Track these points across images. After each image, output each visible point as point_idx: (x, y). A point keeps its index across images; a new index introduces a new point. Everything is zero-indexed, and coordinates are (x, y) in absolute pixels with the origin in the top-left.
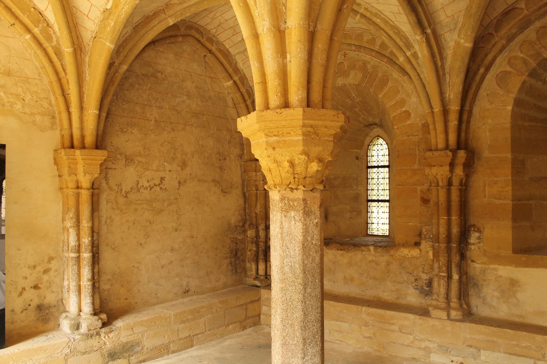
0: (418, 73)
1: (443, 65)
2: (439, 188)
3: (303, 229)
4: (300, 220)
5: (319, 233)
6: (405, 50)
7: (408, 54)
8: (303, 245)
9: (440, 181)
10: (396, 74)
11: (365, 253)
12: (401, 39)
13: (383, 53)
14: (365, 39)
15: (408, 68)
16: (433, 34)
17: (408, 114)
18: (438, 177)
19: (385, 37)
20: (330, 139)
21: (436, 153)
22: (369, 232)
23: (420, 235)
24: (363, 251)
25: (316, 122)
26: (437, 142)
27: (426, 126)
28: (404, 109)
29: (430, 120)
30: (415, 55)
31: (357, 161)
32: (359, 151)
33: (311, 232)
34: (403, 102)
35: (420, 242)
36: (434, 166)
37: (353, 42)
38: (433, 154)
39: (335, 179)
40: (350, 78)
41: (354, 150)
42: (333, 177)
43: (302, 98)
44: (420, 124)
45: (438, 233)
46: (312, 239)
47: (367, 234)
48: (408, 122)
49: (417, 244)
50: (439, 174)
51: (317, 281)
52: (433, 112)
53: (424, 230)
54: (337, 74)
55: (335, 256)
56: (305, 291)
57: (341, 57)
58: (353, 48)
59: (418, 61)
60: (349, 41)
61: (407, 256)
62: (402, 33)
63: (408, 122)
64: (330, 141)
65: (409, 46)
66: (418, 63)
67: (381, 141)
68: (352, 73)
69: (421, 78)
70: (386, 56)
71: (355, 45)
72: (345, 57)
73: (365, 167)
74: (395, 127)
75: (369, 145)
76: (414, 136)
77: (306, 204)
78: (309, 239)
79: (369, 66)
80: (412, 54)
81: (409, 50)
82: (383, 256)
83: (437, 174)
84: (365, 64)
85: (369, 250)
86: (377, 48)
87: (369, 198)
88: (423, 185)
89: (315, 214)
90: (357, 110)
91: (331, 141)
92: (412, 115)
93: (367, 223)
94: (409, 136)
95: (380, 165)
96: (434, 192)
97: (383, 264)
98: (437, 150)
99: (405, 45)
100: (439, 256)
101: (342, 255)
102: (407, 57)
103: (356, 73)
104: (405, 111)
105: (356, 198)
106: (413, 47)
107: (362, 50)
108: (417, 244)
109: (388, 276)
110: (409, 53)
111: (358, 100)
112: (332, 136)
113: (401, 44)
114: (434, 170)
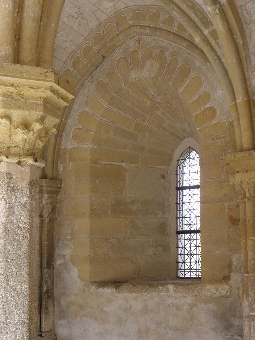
0: (218, 57)
1: (245, 44)
2: (246, 200)
3: (5, 207)
4: (3, 197)
5: (28, 214)
6: (202, 27)
7: (206, 32)
8: (6, 227)
9: (247, 190)
10: (198, 62)
11: (162, 294)
12: (197, 15)
13: (182, 35)
14: (161, 19)
15: (206, 49)
16: (229, 4)
17: (212, 111)
18: (244, 186)
19: (177, 12)
20: (39, 102)
21: (240, 155)
22: (180, 275)
23: (230, 266)
24: (160, 291)
25: (19, 80)
26: (242, 143)
27: (231, 125)
28: (208, 106)
29: (233, 114)
30: (214, 33)
31: (162, 181)
32: (166, 168)
33: (16, 212)
34: (207, 97)
35: (229, 276)
36: (238, 172)
37: (147, 23)
38: (235, 157)
39: (132, 203)
40: (145, 70)
41: (159, 167)
42: (129, 200)
43: (6, 54)
44: (227, 123)
45: (246, 260)
46: (18, 221)
47: (178, 277)
48: (214, 122)
49: (226, 279)
50: (244, 182)
51: (24, 273)
52: (236, 104)
53: (234, 259)
54: (130, 65)
55: (127, 301)
56: (7, 284)
57: (135, 44)
58: (148, 31)
59: (217, 41)
60: (143, 23)
61: (215, 296)
62: (198, 6)
63: (214, 122)
64: (38, 105)
65: (207, 23)
66: (218, 44)
67: (193, 154)
68: (148, 63)
69: (222, 63)
70: (185, 39)
71: (149, 27)
72: (139, 43)
73: (174, 188)
74: (198, 129)
75: (179, 160)
76: (220, 138)
77: (11, 178)
78: (14, 220)
79: (167, 54)
80: (210, 33)
81: (207, 28)
82: (185, 297)
83: (241, 182)
84: (163, 50)
85: (168, 290)
86: (175, 29)
87: (180, 229)
88: (232, 200)
89: (22, 191)
90: (159, 113)
91: (41, 105)
92: (218, 113)
93: (178, 262)
94: (214, 139)
95: (192, 185)
96: (241, 208)
97: (185, 308)
98: (242, 150)
99: (202, 21)
100: (248, 290)
101: (135, 299)
102: (205, 37)
103: (152, 64)
104: (210, 108)
105: (162, 228)
106: (212, 24)
107: (158, 34)
108: (226, 279)
109: (192, 324)
110: (207, 31)
111: (158, 99)
112: (42, 100)
113: (197, 20)
114: (238, 178)
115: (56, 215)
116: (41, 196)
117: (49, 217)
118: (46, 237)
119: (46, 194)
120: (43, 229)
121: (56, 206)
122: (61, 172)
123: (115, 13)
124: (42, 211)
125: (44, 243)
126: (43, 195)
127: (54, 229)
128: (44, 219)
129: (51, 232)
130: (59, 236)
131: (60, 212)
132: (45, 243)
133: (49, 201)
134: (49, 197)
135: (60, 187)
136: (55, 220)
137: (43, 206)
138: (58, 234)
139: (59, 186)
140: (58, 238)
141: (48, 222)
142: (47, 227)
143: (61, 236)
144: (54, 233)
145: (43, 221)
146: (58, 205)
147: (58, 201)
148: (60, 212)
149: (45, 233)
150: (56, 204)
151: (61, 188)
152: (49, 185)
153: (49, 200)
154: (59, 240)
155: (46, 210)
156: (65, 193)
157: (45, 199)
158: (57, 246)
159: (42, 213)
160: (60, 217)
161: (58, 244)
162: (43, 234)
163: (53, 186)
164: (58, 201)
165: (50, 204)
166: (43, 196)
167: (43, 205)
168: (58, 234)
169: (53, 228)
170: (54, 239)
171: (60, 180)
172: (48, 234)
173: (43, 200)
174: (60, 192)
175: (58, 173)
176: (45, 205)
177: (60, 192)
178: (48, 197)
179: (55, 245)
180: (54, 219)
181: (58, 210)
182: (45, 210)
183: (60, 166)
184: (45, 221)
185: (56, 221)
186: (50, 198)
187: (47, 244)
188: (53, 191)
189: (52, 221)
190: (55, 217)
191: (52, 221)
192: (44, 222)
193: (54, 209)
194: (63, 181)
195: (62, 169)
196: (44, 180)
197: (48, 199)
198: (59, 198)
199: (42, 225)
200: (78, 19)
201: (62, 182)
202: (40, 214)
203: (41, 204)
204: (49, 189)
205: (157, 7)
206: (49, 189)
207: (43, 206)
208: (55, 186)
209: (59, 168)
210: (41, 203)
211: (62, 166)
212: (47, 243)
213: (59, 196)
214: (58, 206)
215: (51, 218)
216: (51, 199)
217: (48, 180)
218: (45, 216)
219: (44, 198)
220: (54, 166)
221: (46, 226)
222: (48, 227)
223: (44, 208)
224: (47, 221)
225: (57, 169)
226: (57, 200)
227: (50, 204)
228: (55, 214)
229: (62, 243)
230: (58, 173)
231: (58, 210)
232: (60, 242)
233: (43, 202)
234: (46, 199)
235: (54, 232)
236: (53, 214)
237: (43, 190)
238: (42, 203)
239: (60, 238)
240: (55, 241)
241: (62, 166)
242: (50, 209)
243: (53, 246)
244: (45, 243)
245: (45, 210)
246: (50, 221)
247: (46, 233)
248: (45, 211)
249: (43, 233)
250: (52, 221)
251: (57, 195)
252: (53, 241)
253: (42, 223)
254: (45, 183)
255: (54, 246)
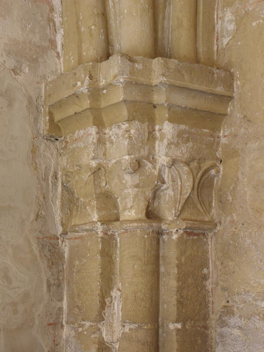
115: (213, 211)
116: (150, 133)
117: (184, 220)
118: (174, 300)
119: (170, 120)
120: (162, 269)
121: (213, 172)
122: (225, 41)
123: (202, 207)
124: (155, 195)
125: (167, 326)
126: (157, 128)
127: (208, 268)
128: (164, 227)
129: (194, 277)
130: (226, 294)
131: (230, 198)
132: (172, 326)
133: (183, 152)
134: (180, 134)
135: (228, 94)
136: (211, 230)
137: (156, 173)
138: (224, 289)
139: (220, 89)
140: (224, 303)
141: (180, 238)
142: (178, 259)
143: (236, 298)
144: (209, 285)
145: (159, 233)
146: (221, 169)
147: (219, 154)
148: (230, 198)
149: (170, 284)
150: (213, 166)
151: (231, 98)
152: (178, 83)
153: (184, 149)
154: (228, 311)
155: (170, 192)
156: (245, 116)
157: (165, 142)
158: (222, 336)
159: (156, 204)
160: (229, 218)
161: (223, 329)
162: (162, 289)
163: (196, 86)
164: (219, 154)
165: (187, 164)
166: (158, 134)
167: (157, 168)
168: (224, 289)
169: (205, 264)
170: (207, 306)
171: (226, 69)
172: (180, 290)
173: (157, 145)
174: (225, 115)
175: (215, 48)
176: (167, 169)
177: (225, 115)
178: (178, 136)
179: (213, 334)
180: (206, 227)
181: (220, 190)
182: (168, 188)
183: (222, 19)
184: (168, 233)
185: (215, 234)
186: (188, 140)
187: (178, 330)
188: (196, 110)
189: (198, 235)
190: (207, 219)
191: (198, 235)
192: (165, 237)
193: (203, 185)
194: (237, 74)
195: (231, 27)
196: (157, 63)
197: (177, 145)
198: (223, 140)
199: (158, 250)
200: (214, 313)
201: (232, 75)
202: (148, 207)
203: (149, 165)
204: (181, 100)
205: (180, 205)
206: (181, 100)
207: (160, 170)
208: (203, 88)
209: (218, 27)
210: (150, 162)
211: (229, 16)
212: (179, 326)
213: (224, 134)
214: (218, 172)
215: (195, 221)
216: (190, 144)
217: (173, 63)
218: (169, 214)
219: (162, 140)
220: (201, 17)
221: (171, 253)
222: (183, 259)
223: (163, 182)
224: (175, 237)
225: (211, 29)
226: (217, 150)
227: (189, 165)
228: (210, 203)
229: (240, 328)
230: (215, 48)
231: (220, 190)
232: (233, 321)
233: (156, 157)
234: (168, 144)
235: (205, 278)
236: (199, 206)
237: (155, 107)
238: (153, 161)
239: (231, 303)
240: (211, 316)
241: (229, 16)
242: (188, 185)
243: (205, 338)
244: (172, 326)
245: (168, 188)
246: (189, 232)
247: (174, 283)
248: (168, 193)
249: (161, 283)
250: (196, 234)
251: (216, 129)
252: (206, 318)
253: (158, 243)
254: (163, 75)
255: (207, 336)
